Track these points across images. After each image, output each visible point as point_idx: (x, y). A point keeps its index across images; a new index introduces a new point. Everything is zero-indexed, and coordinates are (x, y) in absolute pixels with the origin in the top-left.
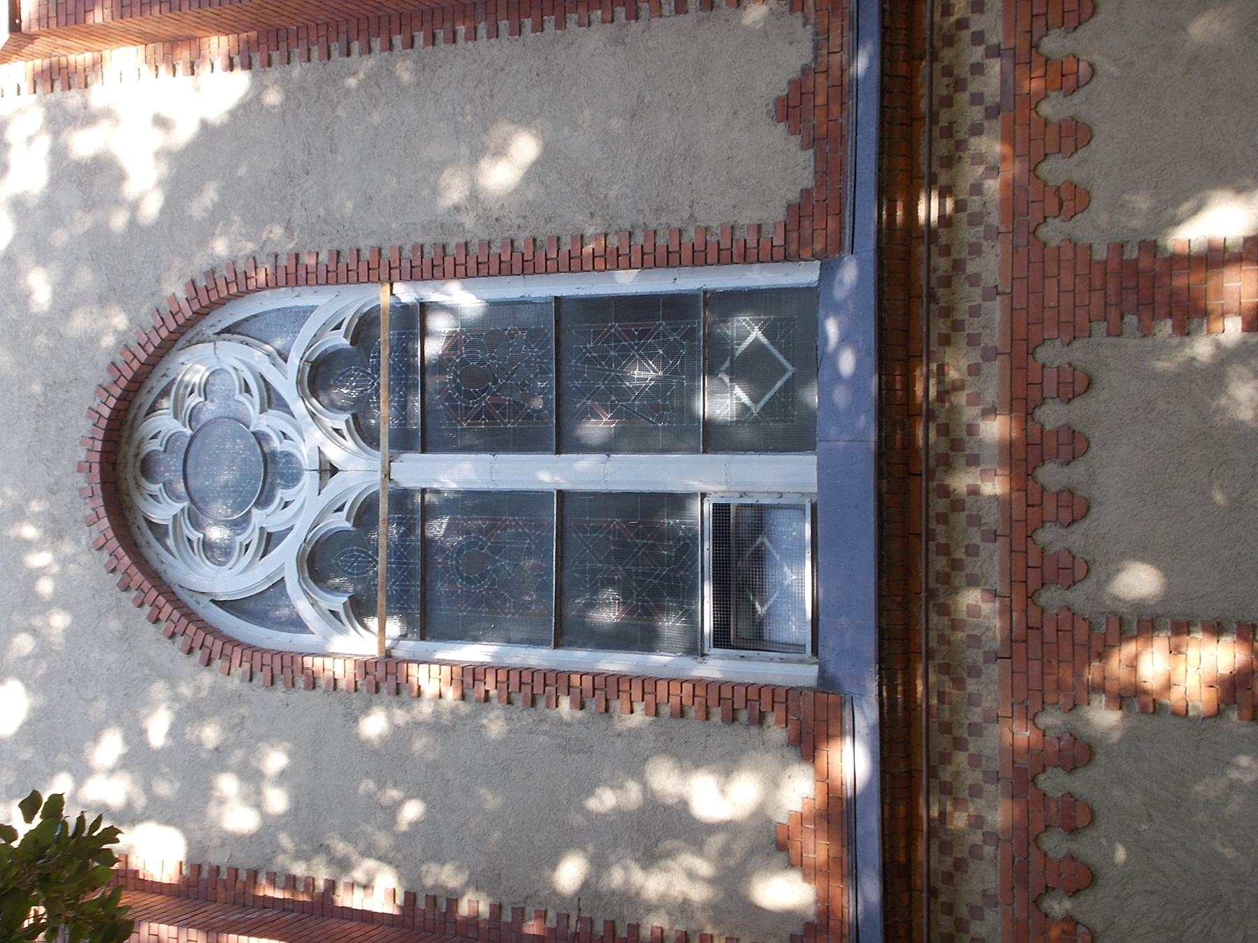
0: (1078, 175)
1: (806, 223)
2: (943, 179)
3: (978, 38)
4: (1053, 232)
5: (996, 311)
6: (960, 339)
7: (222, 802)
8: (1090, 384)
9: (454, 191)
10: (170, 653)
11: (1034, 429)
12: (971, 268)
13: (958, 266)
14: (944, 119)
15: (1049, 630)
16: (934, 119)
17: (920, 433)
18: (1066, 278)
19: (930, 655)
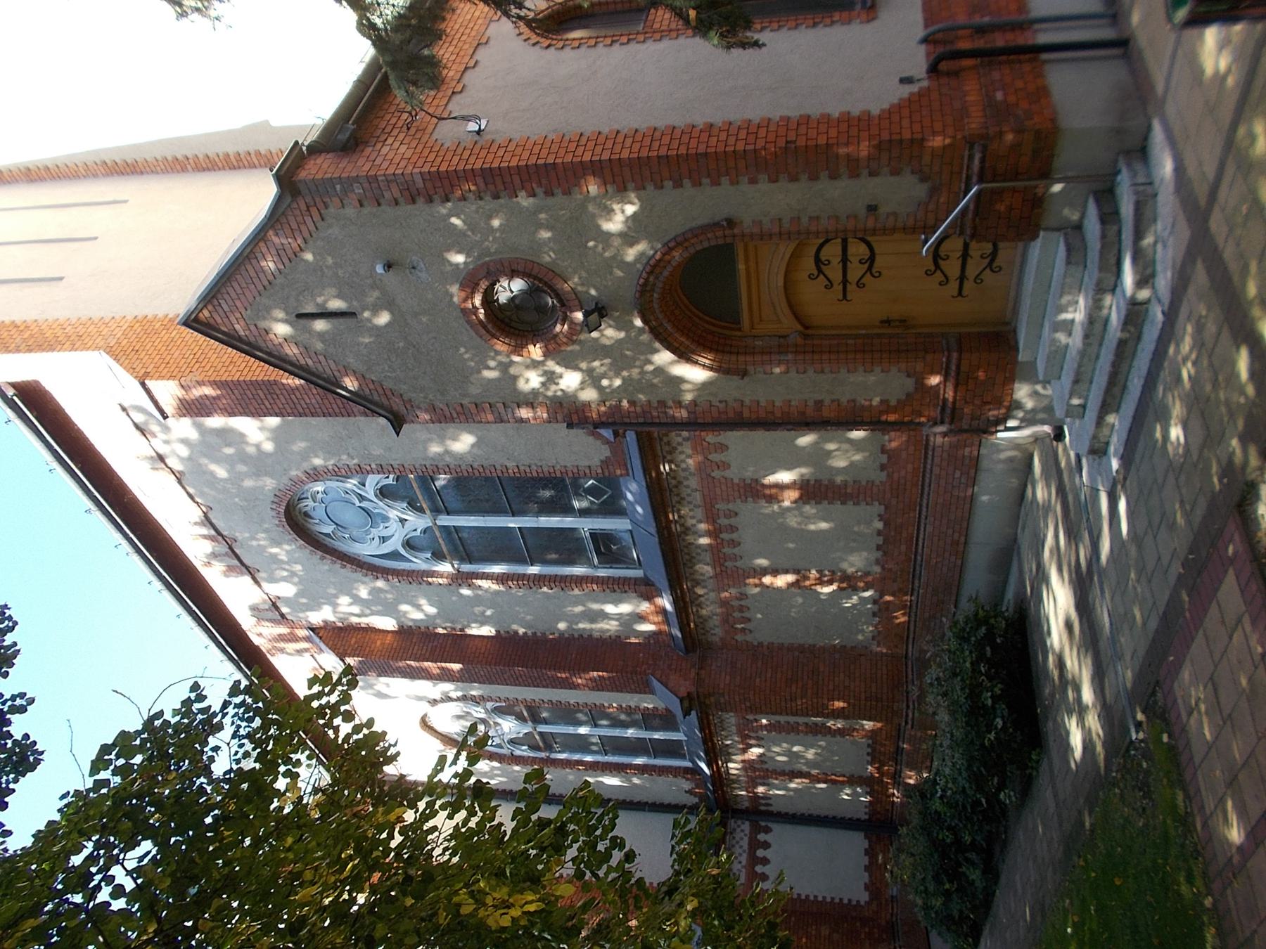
0: (723, 441)
1: (611, 467)
2: (669, 457)
3: (742, 831)
4: (716, 474)
5: (698, 495)
6: (685, 502)
7: (268, 439)
8: (736, 514)
9: (435, 449)
10: (359, 575)
11: (717, 526)
12: (685, 483)
13: (680, 483)
14: (665, 439)
15: (729, 572)
16: (661, 440)
17: (662, 467)
18: (724, 487)
19: (673, 507)
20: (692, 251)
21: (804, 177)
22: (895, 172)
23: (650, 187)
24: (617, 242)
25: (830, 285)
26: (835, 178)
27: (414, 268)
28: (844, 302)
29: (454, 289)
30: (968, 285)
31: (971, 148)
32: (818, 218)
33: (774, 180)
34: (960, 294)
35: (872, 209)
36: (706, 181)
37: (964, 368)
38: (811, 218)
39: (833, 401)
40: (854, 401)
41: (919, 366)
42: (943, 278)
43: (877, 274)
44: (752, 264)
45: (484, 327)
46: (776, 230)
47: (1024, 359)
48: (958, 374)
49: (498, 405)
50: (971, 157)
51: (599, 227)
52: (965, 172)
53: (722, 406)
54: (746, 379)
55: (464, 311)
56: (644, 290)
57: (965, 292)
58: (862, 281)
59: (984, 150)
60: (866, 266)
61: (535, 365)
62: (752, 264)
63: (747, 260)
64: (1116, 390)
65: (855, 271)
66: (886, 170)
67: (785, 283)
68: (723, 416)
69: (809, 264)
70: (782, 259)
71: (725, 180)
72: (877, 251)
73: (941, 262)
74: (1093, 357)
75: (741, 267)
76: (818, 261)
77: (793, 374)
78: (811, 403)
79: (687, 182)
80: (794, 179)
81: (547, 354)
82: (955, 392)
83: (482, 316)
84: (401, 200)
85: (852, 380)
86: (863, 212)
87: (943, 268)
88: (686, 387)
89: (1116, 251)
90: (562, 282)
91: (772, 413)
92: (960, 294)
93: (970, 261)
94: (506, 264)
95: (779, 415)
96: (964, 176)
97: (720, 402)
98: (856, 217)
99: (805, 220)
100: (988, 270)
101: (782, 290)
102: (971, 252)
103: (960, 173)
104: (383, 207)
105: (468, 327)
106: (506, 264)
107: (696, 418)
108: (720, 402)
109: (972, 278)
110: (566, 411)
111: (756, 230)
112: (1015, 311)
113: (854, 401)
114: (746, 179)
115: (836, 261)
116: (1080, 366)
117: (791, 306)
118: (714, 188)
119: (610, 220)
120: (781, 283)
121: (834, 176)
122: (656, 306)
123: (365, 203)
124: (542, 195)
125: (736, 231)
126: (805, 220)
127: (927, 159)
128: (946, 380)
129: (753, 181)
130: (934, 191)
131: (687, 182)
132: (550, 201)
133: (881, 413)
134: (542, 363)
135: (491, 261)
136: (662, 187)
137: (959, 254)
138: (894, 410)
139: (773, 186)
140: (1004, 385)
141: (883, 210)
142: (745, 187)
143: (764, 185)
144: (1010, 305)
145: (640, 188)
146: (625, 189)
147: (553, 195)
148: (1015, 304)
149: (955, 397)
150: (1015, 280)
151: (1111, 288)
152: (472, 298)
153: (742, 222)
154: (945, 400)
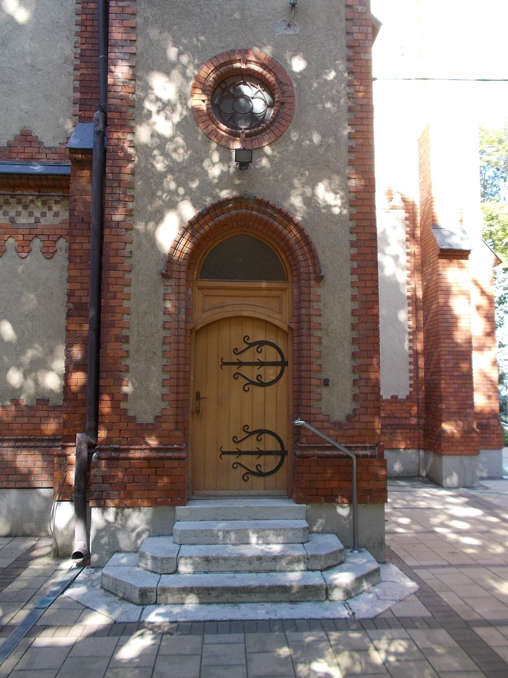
16: (13, 196)
20: (296, 247)
21: (355, 334)
22: (355, 398)
23: (352, 224)
24: (308, 191)
25: (236, 352)
26: (353, 357)
27: (289, 25)
28: (221, 364)
29: (267, 52)
30: (233, 458)
31: (372, 448)
32: (321, 343)
33: (354, 313)
34: (224, 453)
35: (326, 383)
36: (355, 264)
37: (168, 463)
38: (320, 338)
39: (128, 352)
40: (127, 370)
41: (169, 426)
42: (239, 439)
43: (246, 388)
44: (265, 293)
45: (225, 64)
46: (312, 312)
47: (177, 512)
48: (161, 459)
49: (134, 48)
50: (365, 448)
51: (320, 180)
52: (355, 445)
53: (126, 252)
54: (158, 278)
55: (246, 52)
56: (263, 205)
57: (225, 457)
58: (239, 376)
59: (372, 456)
60: (255, 380)
61: (183, 98)
62: (265, 293)
63: (268, 289)
64: (227, 596)
65: (251, 373)
66: (357, 391)
67: (242, 317)
68: (112, 253)
69: (260, 335)
70: (269, 316)
71: (355, 278)
72: (268, 388)
73: (255, 436)
74: (237, 568)
75: (264, 285)
76: (262, 343)
77: (162, 318)
78: (125, 332)
79: (355, 251)
80: (354, 327)
81: (195, 111)
82: (140, 459)
83: (238, 65)
84: (350, 37)
85: (154, 368)
86: (324, 376)
87: (250, 437)
88: (151, 225)
89: (335, 563)
90: (270, 141)
91: (115, 298)
92: (224, 453)
93: (255, 457)
94: (290, 100)
95: (112, 303)
96: (351, 445)
97: (131, 252)
98: (320, 371)
99: (319, 334)
100: (244, 471)
101: (239, 314)
102: (262, 457)
103: (353, 443)
104: (345, 22)
105: (228, 49)
106: (290, 100)
107: (111, 228)
108: (131, 252)
109: (238, 460)
110: (124, 109)
111: (313, 297)
112: (206, 497)
113: (127, 370)
114: (356, 293)
115: (261, 357)
116: (225, 559)
117: (218, 321)
118: (349, 270)
119: (326, 190)
120: (245, 314)
121: (354, 355)
122: (244, 211)
123: (348, 10)
124: (350, 144)
125: (312, 282)
126: (319, 334)
127: (364, 418)
128: (151, 449)
129: (354, 298)
130: (339, 425)
131: (355, 251)
132: (344, 149)
133: (112, 395)
134: (184, 103)
135: (293, 87)
136: (351, 233)
137: (262, 449)
138: (115, 405)
139: (349, 312)
140: (148, 498)
141: (324, 391)
142: (349, 292)
143: (349, 306)
144: (210, 492)
145: (352, 217)
146: (351, 206)
147: (349, 152)
148: (211, 496)
149: (133, 459)
150: (236, 493)
151: (310, 568)
152: (256, 63)
153: (320, 287)
154: (128, 450)
